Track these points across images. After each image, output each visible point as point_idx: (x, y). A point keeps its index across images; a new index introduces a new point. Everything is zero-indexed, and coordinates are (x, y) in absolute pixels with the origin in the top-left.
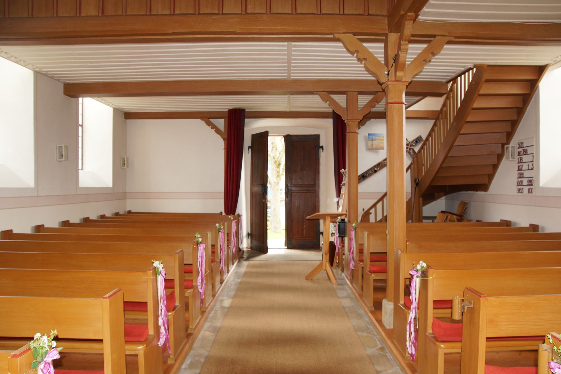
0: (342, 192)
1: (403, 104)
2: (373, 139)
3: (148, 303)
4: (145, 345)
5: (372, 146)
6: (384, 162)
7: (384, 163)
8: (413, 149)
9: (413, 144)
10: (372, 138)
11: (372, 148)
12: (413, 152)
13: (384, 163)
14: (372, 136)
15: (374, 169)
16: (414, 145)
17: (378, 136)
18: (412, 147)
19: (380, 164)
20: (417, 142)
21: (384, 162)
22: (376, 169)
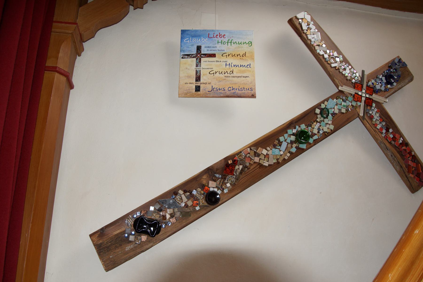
0: (335, 100)
1: (57, 75)
2: (204, 51)
3: (182, 29)
4: (391, 79)
5: (198, 79)
6: (257, 155)
7: (257, 159)
8: (379, 106)
9: (378, 87)
10: (199, 48)
11: (198, 89)
12: (382, 120)
13: (257, 159)
14: (197, 42)
15: (203, 187)
16: (383, 88)
17: (226, 40)
18: (375, 97)
19: (235, 162)
20: (389, 78)
21: (257, 155)
22: (212, 186)
